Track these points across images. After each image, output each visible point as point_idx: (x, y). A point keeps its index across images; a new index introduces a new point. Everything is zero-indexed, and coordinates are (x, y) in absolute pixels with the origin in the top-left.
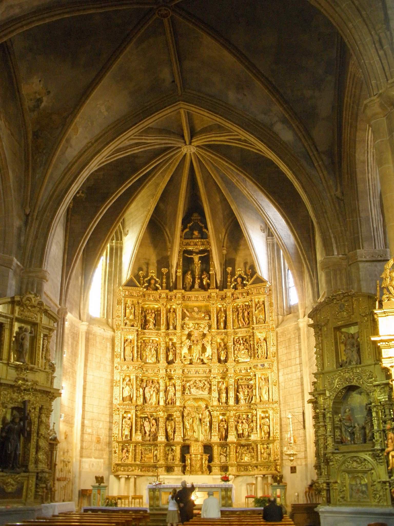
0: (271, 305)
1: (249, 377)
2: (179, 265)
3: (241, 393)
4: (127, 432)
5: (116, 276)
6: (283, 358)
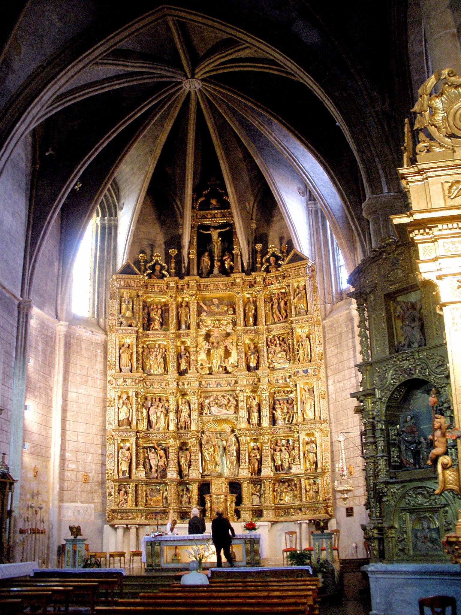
0: (315, 290)
1: (289, 389)
2: (193, 244)
3: (279, 411)
4: (124, 467)
5: (110, 263)
6: (332, 360)
